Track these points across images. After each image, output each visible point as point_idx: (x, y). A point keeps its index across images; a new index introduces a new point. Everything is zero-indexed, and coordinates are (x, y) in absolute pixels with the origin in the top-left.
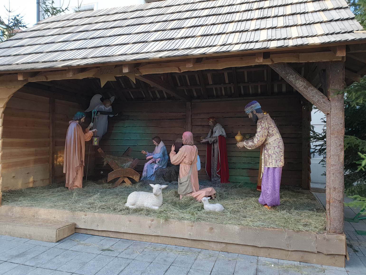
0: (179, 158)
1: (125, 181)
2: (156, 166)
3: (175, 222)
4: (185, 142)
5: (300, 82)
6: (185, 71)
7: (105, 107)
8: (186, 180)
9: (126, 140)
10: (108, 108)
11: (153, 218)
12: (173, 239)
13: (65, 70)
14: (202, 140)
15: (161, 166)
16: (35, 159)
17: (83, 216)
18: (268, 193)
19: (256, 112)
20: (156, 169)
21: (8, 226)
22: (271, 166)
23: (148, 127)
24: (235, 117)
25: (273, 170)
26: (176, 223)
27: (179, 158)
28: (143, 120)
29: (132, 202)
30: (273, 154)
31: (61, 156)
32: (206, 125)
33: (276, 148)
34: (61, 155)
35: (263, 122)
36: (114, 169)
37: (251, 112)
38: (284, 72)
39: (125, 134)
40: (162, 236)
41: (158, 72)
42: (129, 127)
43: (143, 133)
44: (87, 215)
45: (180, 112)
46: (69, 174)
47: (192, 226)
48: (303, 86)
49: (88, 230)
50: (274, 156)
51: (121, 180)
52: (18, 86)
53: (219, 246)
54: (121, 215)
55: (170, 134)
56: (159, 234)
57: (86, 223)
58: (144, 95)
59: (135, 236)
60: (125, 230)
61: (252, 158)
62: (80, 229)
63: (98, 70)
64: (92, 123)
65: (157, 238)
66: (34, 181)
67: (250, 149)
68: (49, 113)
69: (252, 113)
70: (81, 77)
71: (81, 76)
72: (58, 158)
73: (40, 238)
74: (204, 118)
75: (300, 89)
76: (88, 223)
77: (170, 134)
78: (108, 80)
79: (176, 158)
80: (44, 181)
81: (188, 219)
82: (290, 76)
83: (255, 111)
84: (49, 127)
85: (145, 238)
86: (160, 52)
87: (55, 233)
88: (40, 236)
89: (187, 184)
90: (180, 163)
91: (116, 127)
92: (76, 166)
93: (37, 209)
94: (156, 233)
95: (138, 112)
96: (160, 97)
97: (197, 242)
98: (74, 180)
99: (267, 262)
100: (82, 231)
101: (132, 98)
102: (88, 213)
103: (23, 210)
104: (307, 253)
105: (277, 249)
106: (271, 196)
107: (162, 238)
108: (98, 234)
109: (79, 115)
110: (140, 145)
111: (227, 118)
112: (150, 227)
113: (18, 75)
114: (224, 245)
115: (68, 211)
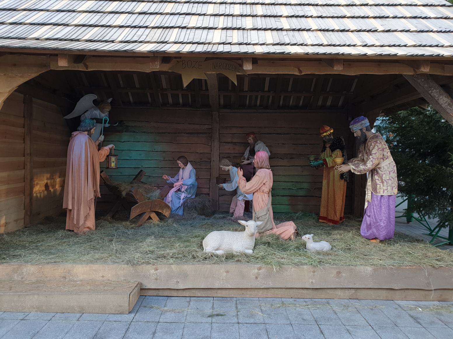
0: (255, 185)
1: (151, 217)
2: (183, 196)
3: (291, 269)
4: (260, 165)
5: (444, 98)
6: (306, 73)
7: (101, 112)
8: (265, 213)
9: (123, 160)
10: (104, 116)
11: (259, 266)
12: (288, 290)
13: (149, 57)
14: (243, 162)
15: (189, 196)
16: (7, 189)
17: (152, 271)
18: (381, 226)
19: (366, 130)
20: (184, 200)
21: (36, 297)
22: (386, 194)
23: (157, 142)
24: (274, 134)
25: (389, 198)
26: (293, 269)
27: (255, 185)
28: (150, 132)
29: (215, 245)
30: (389, 180)
31: (39, 184)
32: (237, 143)
33: (391, 173)
34: (38, 183)
35: (378, 142)
36: (139, 202)
37: (360, 130)
38: (426, 85)
39: (122, 152)
40: (273, 288)
41: (270, 72)
42: (129, 141)
43: (151, 151)
44: (158, 270)
45: (204, 125)
46: (79, 211)
47: (314, 272)
48: (447, 103)
49: (161, 290)
50: (390, 182)
51: (146, 216)
52: (30, 74)
53: (348, 293)
54: (213, 265)
55: (189, 153)
56: (271, 285)
57: (158, 281)
58: (150, 99)
59: (235, 291)
60: (220, 284)
61: (293, 183)
62: (146, 291)
63: (178, 61)
64: (102, 135)
65: (265, 290)
66: (6, 223)
67: (358, 173)
68: (24, 118)
69: (361, 132)
70: (148, 70)
71: (352, 72)
72: (34, 187)
73: (100, 310)
74: (235, 134)
75: (443, 106)
76: (161, 281)
77: (189, 153)
78: (195, 78)
79: (251, 186)
80: (18, 222)
81: (306, 264)
82: (433, 90)
83: (365, 129)
84: (24, 139)
85: (248, 293)
86: (60, 40)
87: (126, 299)
88: (101, 307)
89: (266, 218)
90: (255, 192)
91: (108, 141)
92: (90, 198)
93: (68, 266)
94: (266, 284)
95: (142, 121)
96: (172, 103)
97: (320, 291)
98: (86, 218)
99: (412, 306)
100: (150, 293)
101: (130, 101)
102: (161, 266)
103: (43, 270)
104: (446, 291)
105: (375, 288)
106: (385, 229)
107: (273, 290)
108: (176, 294)
109: (89, 124)
110: (145, 168)
111: (265, 134)
112: (257, 278)
113: (59, 58)
114: (353, 291)
115: (126, 266)
